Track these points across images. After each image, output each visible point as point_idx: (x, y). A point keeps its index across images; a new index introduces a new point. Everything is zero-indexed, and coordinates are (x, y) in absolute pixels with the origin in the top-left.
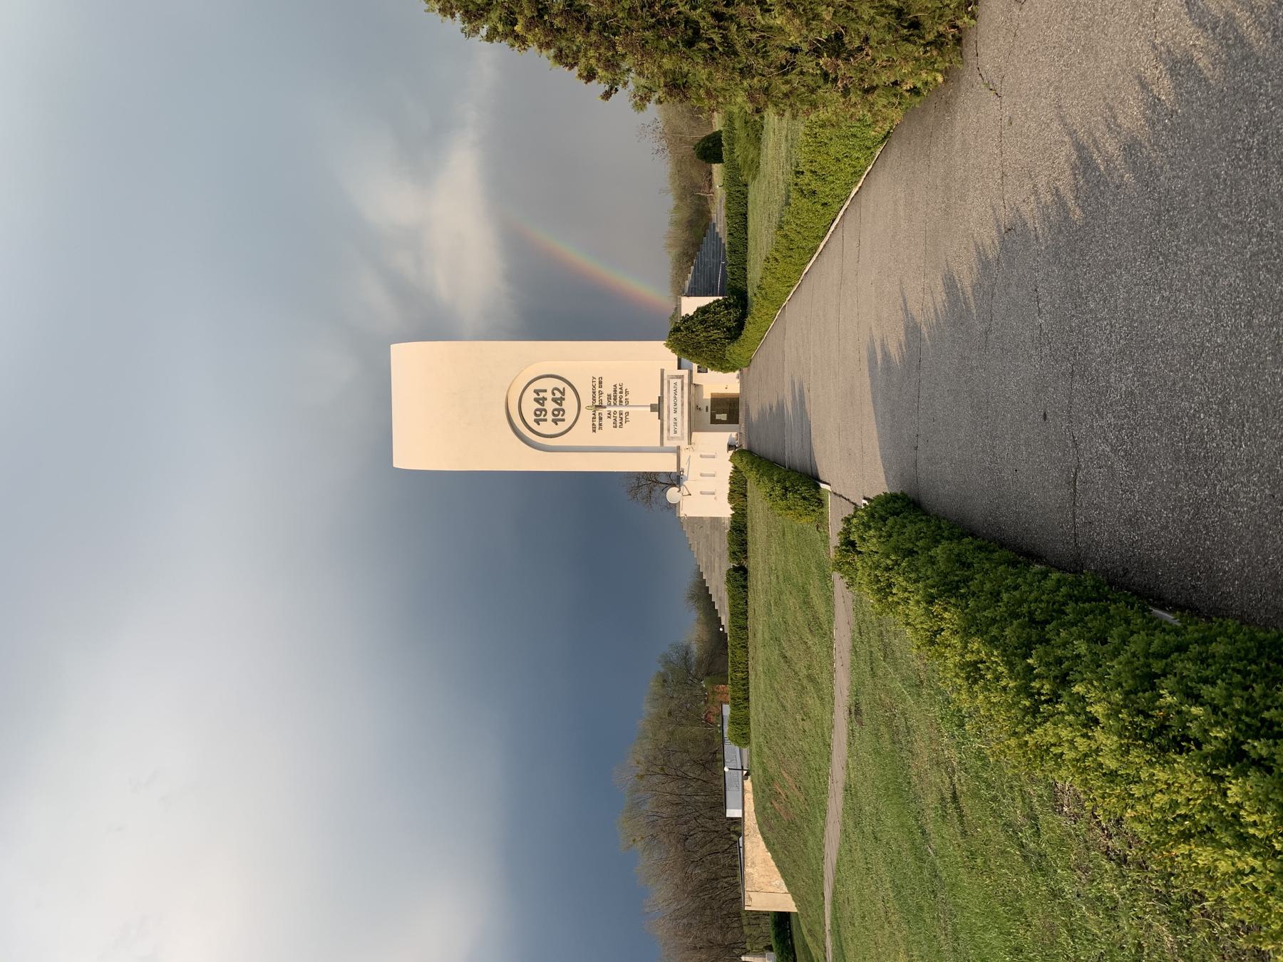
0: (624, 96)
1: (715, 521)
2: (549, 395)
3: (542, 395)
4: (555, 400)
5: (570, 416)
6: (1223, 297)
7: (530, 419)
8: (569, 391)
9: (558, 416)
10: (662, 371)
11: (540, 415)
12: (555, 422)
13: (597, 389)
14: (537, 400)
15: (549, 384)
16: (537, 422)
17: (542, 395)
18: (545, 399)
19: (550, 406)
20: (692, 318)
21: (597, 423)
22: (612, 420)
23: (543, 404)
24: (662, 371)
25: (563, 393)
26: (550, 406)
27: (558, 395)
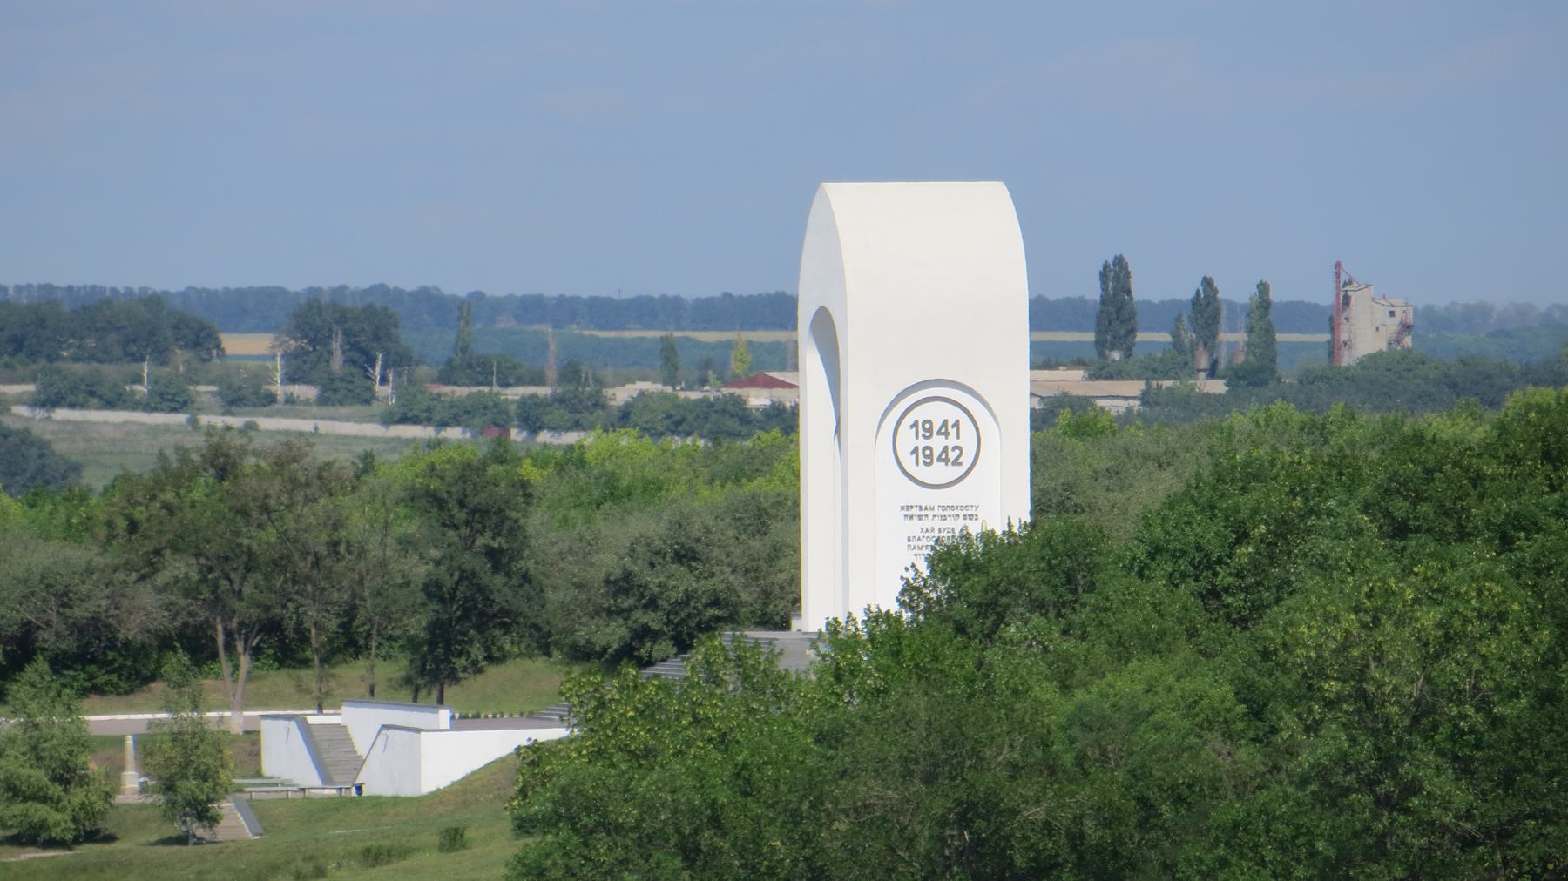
0: (860, 617)
1: (1082, 301)
2: (952, 441)
3: (953, 432)
4: (946, 449)
5: (967, 460)
6: (839, 696)
7: (920, 414)
8: (960, 470)
9: (926, 456)
10: (1338, 265)
11: (926, 428)
12: (915, 451)
13: (962, 514)
14: (945, 423)
15: (968, 441)
16: (915, 425)
17: (953, 432)
18: (947, 434)
19: (937, 443)
20: (1033, 525)
21: (914, 512)
22: (918, 534)
23: (939, 433)
24: (1338, 265)
25: (956, 463)
26: (937, 443)
27: (952, 455)
